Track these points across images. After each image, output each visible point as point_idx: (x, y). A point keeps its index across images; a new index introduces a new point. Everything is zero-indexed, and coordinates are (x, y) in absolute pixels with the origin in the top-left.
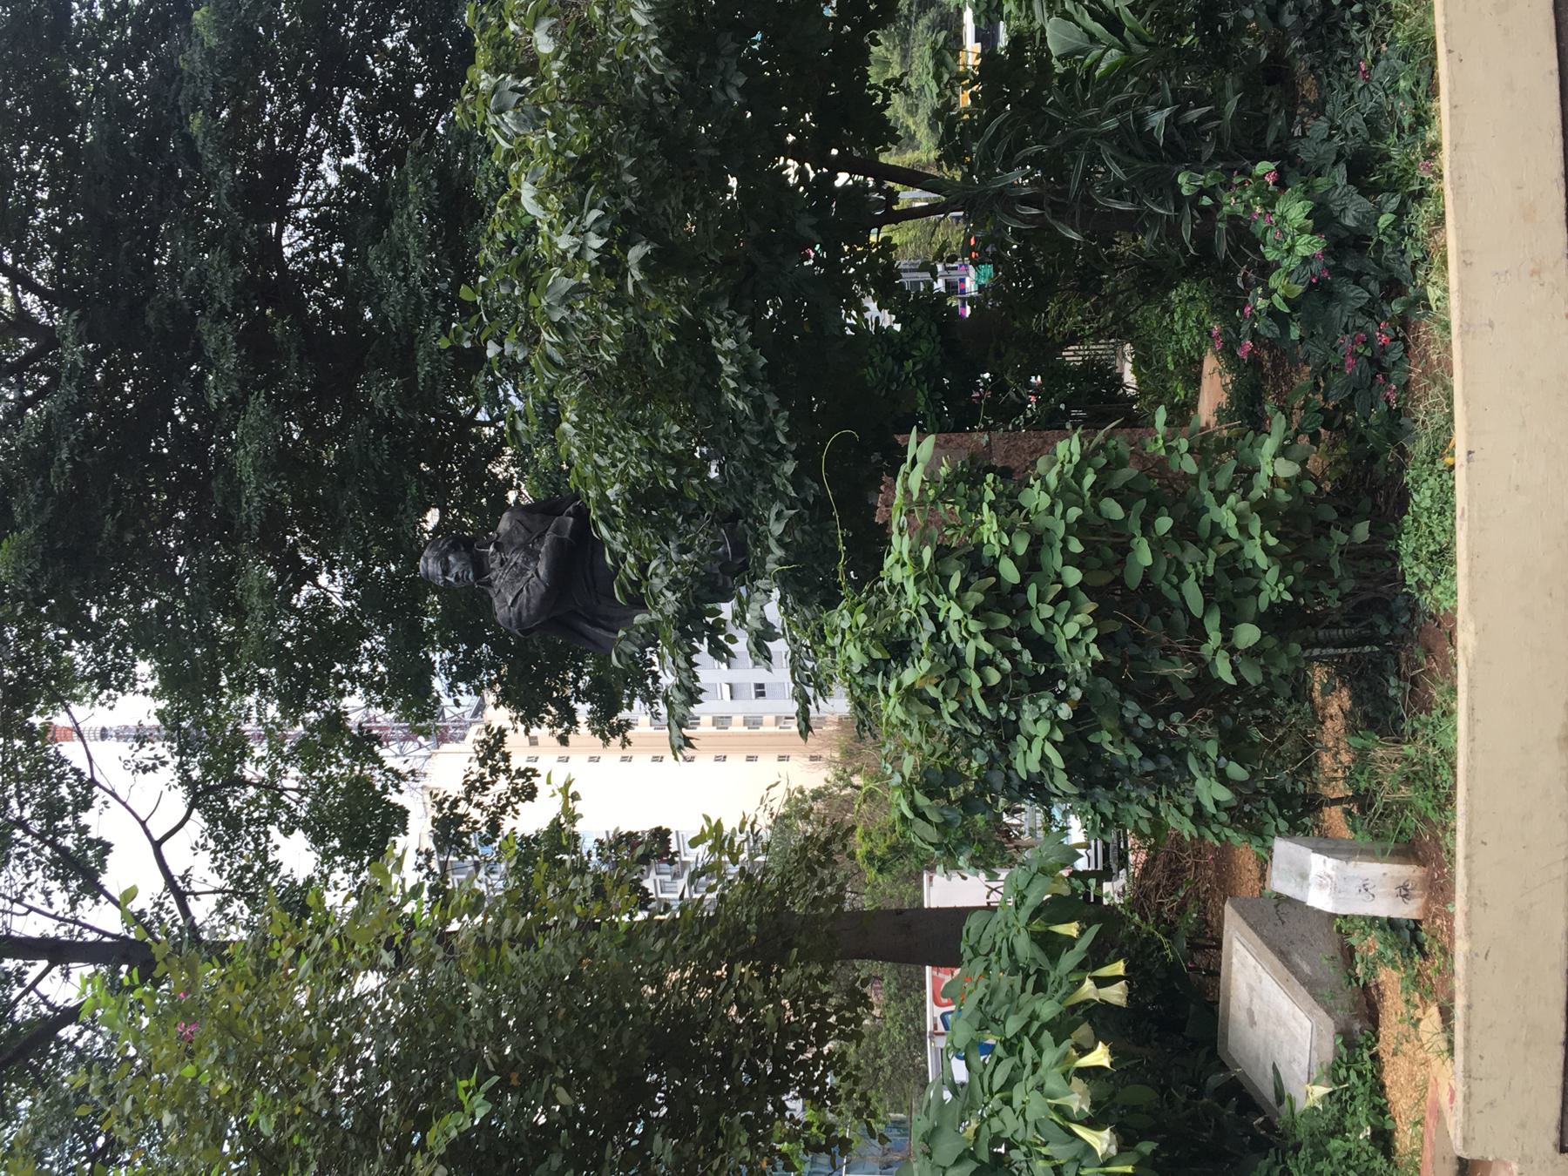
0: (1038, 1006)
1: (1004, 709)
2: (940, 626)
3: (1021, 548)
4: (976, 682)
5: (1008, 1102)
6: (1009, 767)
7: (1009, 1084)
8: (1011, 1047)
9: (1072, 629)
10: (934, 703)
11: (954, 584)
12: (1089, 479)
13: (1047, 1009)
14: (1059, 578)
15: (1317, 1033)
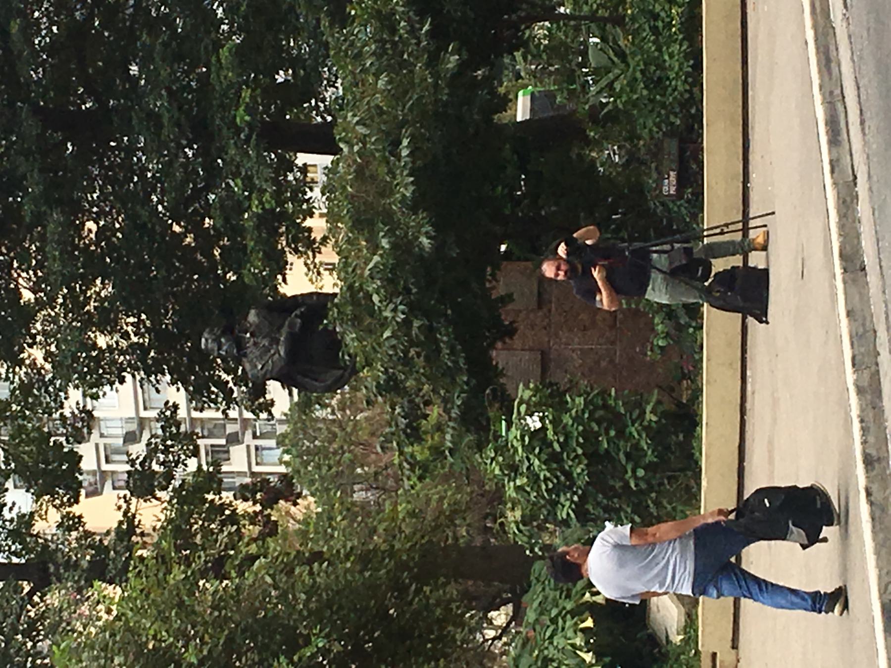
0: (565, 605)
1: (554, 496)
2: (531, 465)
3: (561, 440)
4: (544, 487)
5: (551, 643)
6: (556, 514)
7: (551, 637)
8: (554, 621)
9: (579, 470)
10: (529, 493)
11: (537, 450)
12: (586, 415)
13: (569, 606)
14: (575, 451)
15: (679, 614)
